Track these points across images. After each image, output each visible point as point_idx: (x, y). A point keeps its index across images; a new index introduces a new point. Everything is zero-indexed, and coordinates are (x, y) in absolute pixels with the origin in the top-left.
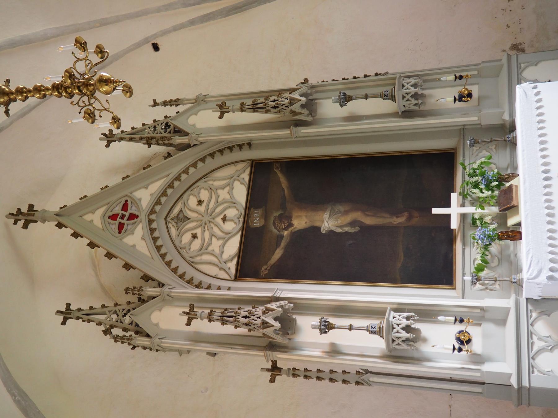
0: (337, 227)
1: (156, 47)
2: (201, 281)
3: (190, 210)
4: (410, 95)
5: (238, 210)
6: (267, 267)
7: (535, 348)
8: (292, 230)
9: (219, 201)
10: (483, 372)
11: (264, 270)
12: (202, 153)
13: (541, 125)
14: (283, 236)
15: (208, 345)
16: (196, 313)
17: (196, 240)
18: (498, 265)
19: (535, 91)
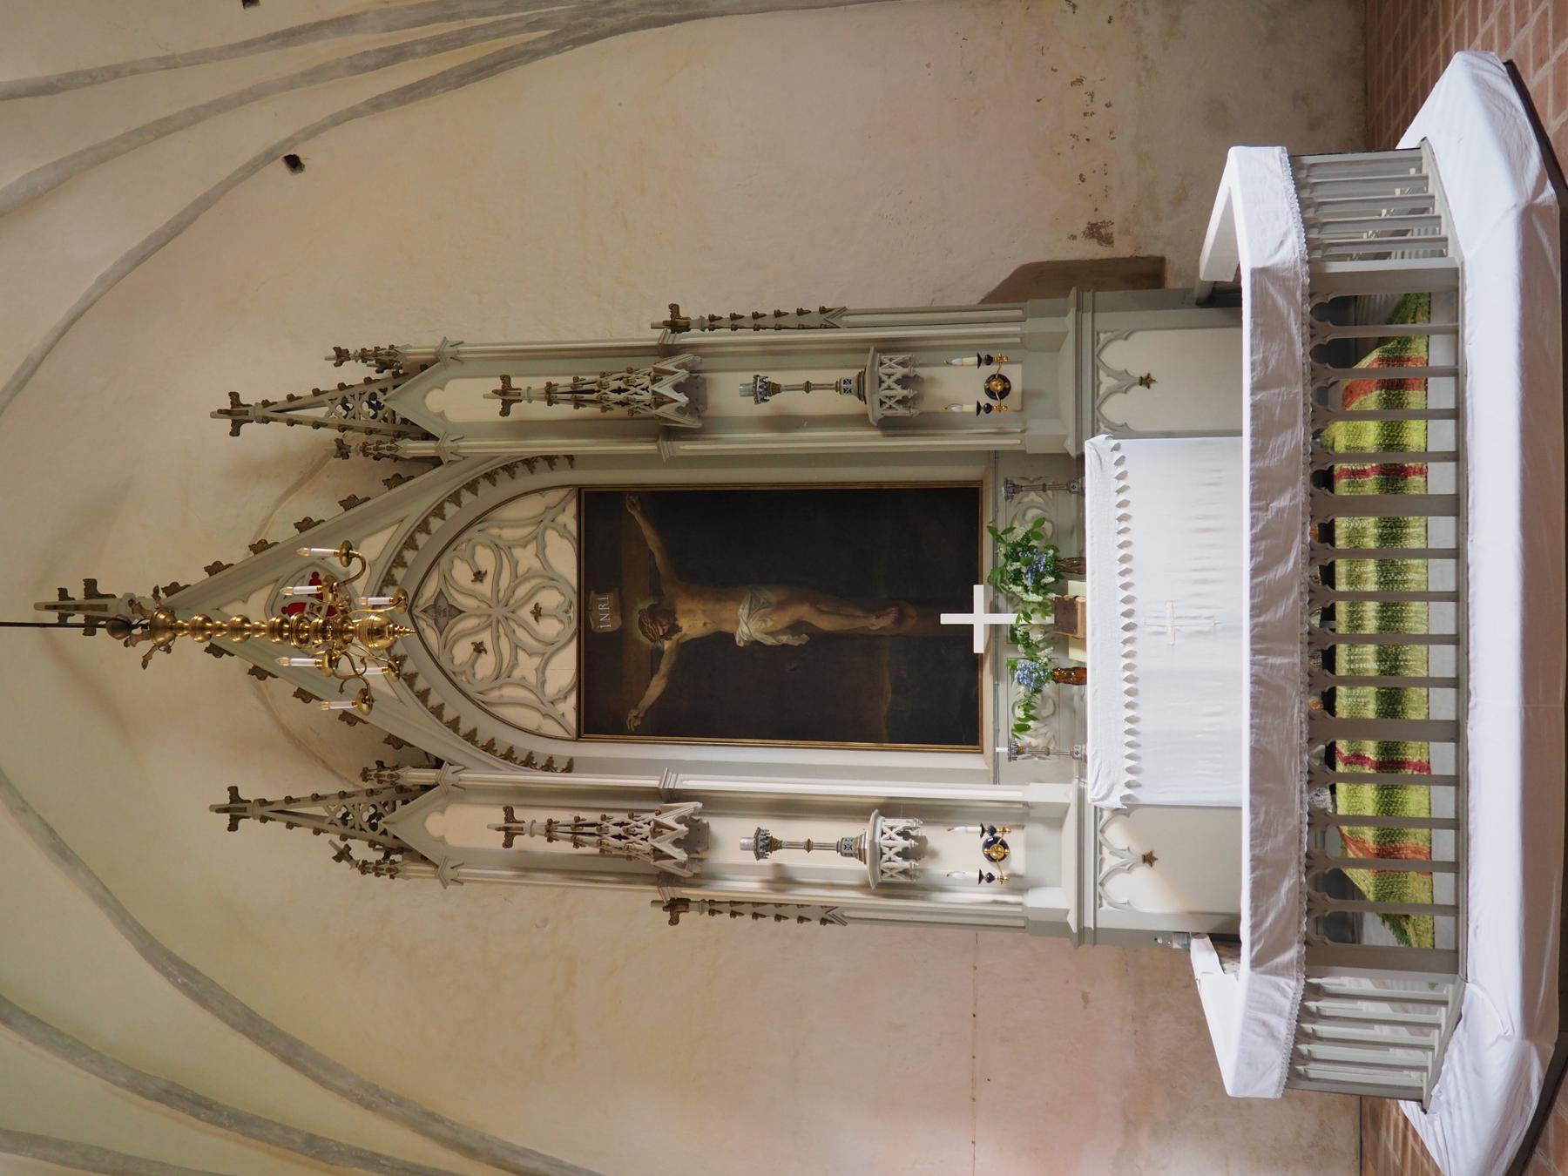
0: (767, 634)
1: (294, 163)
2: (511, 748)
4: (894, 378)
5: (562, 594)
6: (637, 712)
7: (1106, 868)
8: (678, 640)
9: (518, 575)
10: (1026, 908)
11: (633, 718)
12: (466, 475)
13: (1124, 525)
14: (663, 652)
15: (550, 876)
16: (520, 825)
17: (483, 654)
18: (1053, 714)
19: (1117, 455)
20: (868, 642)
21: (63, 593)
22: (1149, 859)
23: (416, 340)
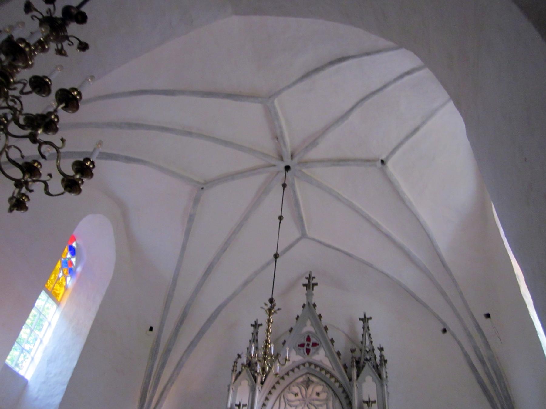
1: (444, 331)
3: (313, 389)
21: (314, 278)
23: (390, 370)
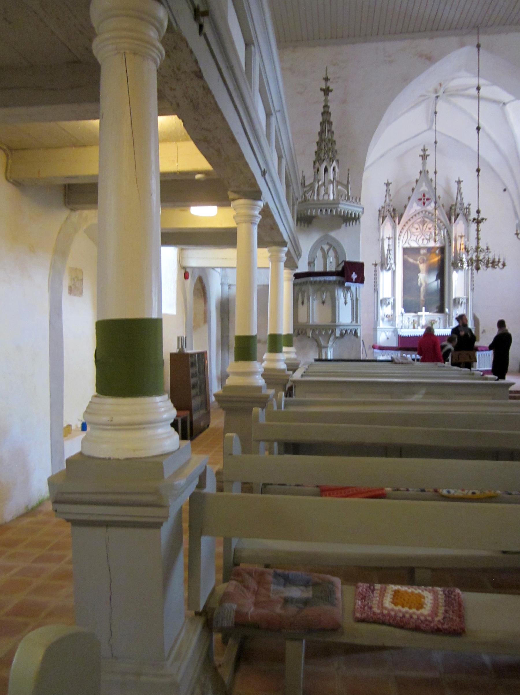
1: (505, 190)
7: (386, 332)
11: (406, 256)
20: (419, 296)
22: (388, 338)
